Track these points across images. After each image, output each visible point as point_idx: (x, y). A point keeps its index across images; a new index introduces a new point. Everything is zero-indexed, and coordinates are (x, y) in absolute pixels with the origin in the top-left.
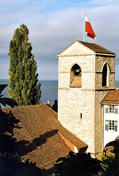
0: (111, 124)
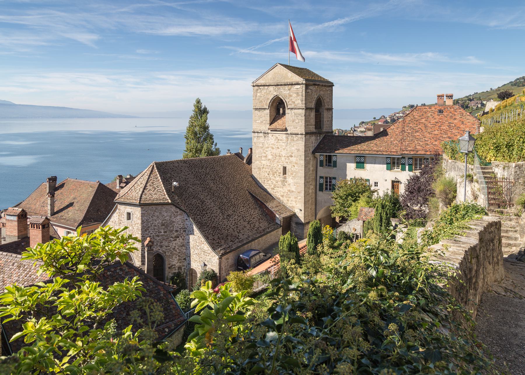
0: (326, 182)
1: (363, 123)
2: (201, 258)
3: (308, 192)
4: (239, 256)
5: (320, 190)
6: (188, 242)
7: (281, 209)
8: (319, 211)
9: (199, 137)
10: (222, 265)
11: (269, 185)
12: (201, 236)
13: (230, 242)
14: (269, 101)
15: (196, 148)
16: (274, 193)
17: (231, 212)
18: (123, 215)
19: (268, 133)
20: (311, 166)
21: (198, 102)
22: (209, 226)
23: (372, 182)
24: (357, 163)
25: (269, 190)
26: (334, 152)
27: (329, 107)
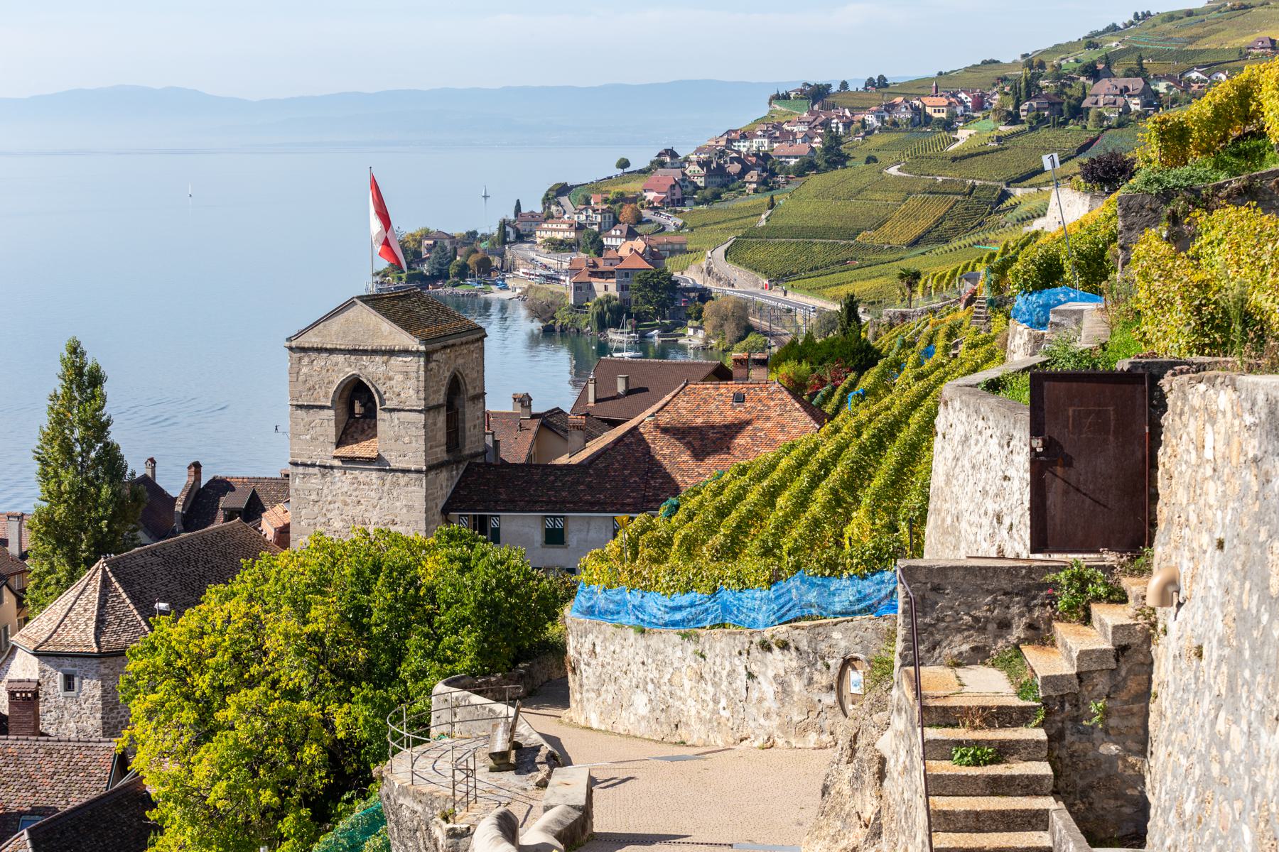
1: (563, 190)
18: (54, 681)
21: (75, 350)
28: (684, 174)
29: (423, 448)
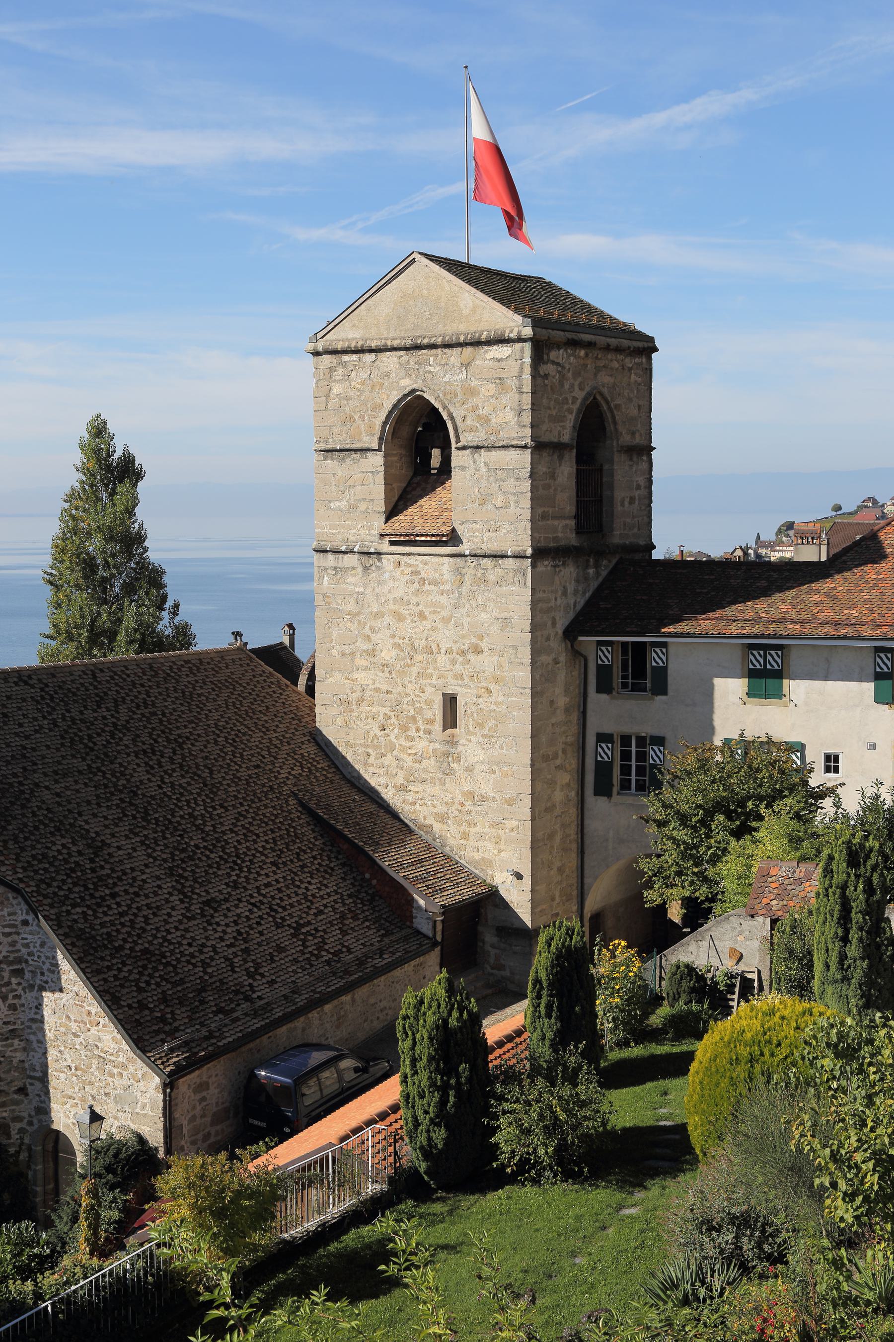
0: (625, 756)
2: (91, 1083)
3: (549, 798)
4: (253, 1076)
5: (597, 793)
6: (33, 1020)
7: (436, 872)
8: (596, 878)
9: (104, 580)
10: (177, 1115)
11: (387, 773)
12: (84, 991)
13: (216, 1013)
14: (382, 416)
15: (92, 625)
16: (407, 807)
17: (217, 889)
19: (379, 554)
20: (559, 690)
21: (99, 430)
22: (121, 948)
23: (815, 757)
24: (753, 674)
25: (388, 795)
26: (657, 631)
27: (638, 440)
28: (883, 513)
29: (528, 514)
